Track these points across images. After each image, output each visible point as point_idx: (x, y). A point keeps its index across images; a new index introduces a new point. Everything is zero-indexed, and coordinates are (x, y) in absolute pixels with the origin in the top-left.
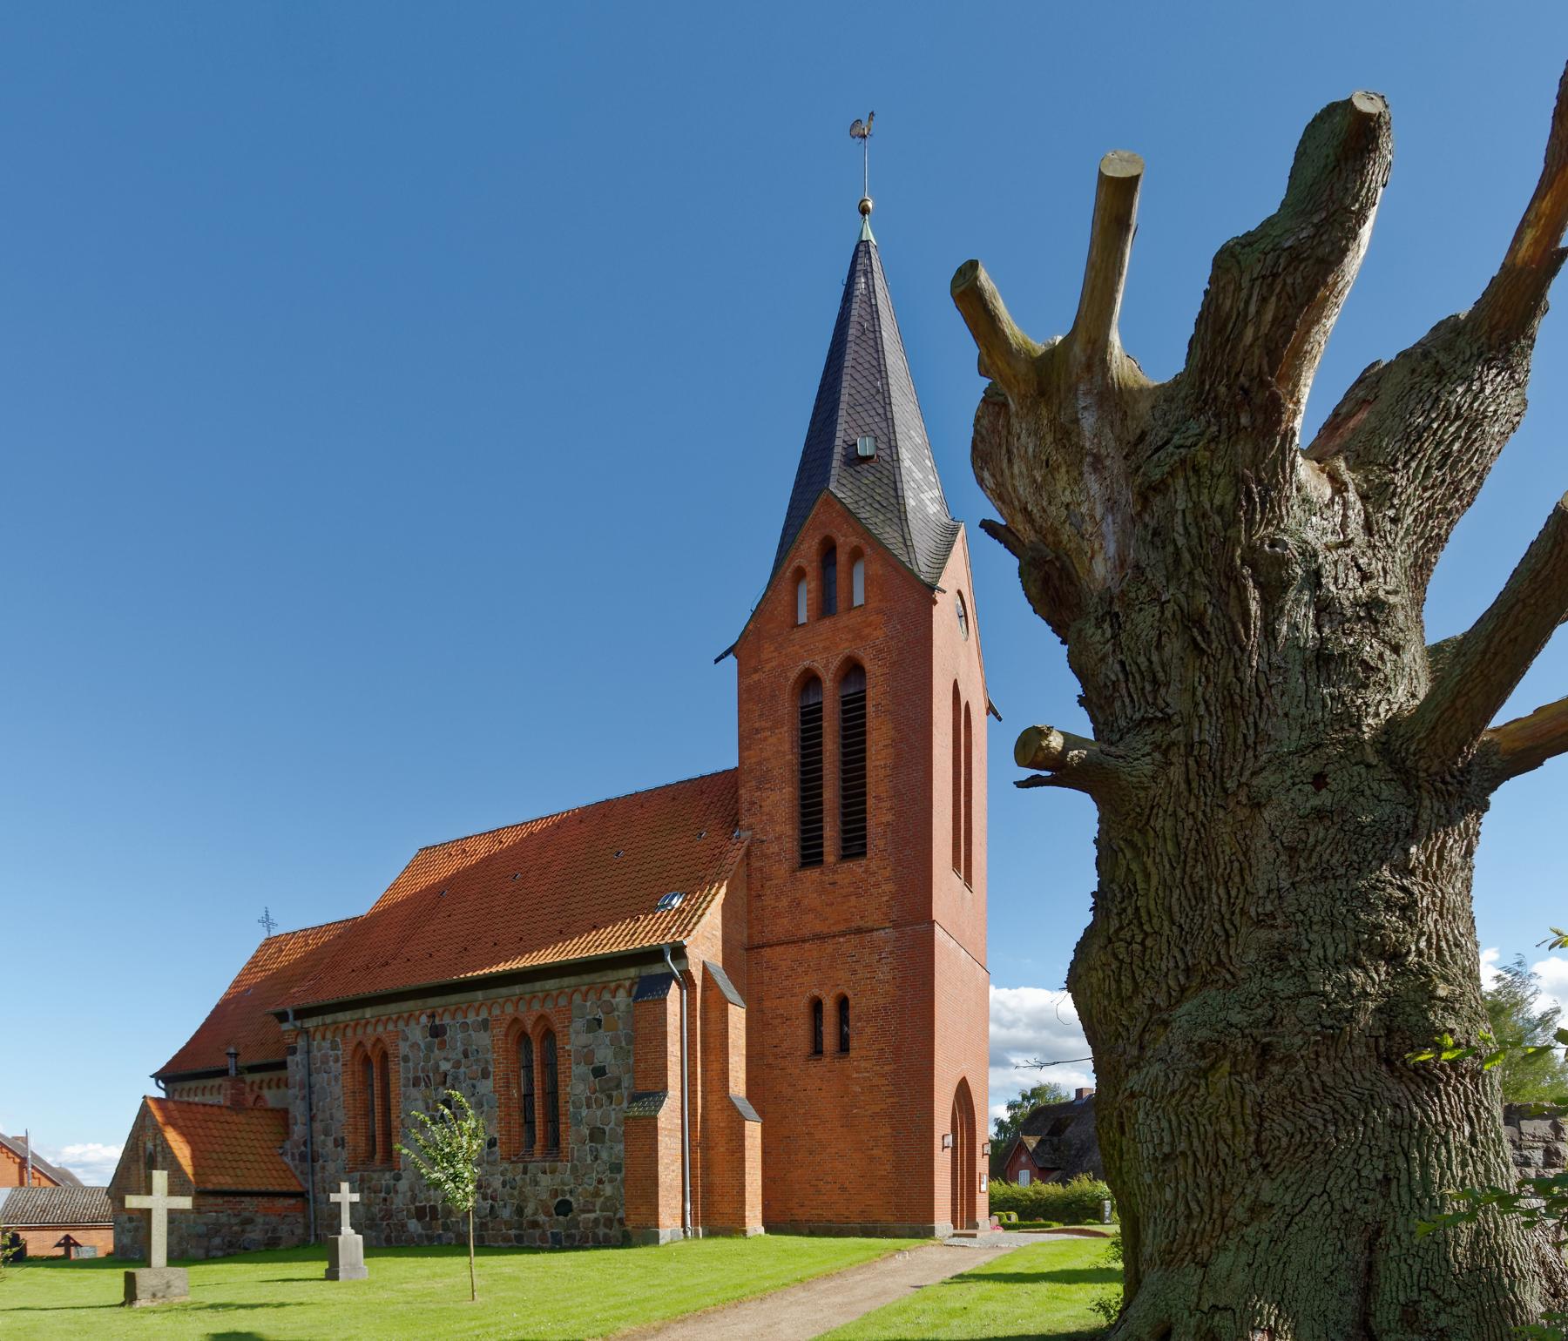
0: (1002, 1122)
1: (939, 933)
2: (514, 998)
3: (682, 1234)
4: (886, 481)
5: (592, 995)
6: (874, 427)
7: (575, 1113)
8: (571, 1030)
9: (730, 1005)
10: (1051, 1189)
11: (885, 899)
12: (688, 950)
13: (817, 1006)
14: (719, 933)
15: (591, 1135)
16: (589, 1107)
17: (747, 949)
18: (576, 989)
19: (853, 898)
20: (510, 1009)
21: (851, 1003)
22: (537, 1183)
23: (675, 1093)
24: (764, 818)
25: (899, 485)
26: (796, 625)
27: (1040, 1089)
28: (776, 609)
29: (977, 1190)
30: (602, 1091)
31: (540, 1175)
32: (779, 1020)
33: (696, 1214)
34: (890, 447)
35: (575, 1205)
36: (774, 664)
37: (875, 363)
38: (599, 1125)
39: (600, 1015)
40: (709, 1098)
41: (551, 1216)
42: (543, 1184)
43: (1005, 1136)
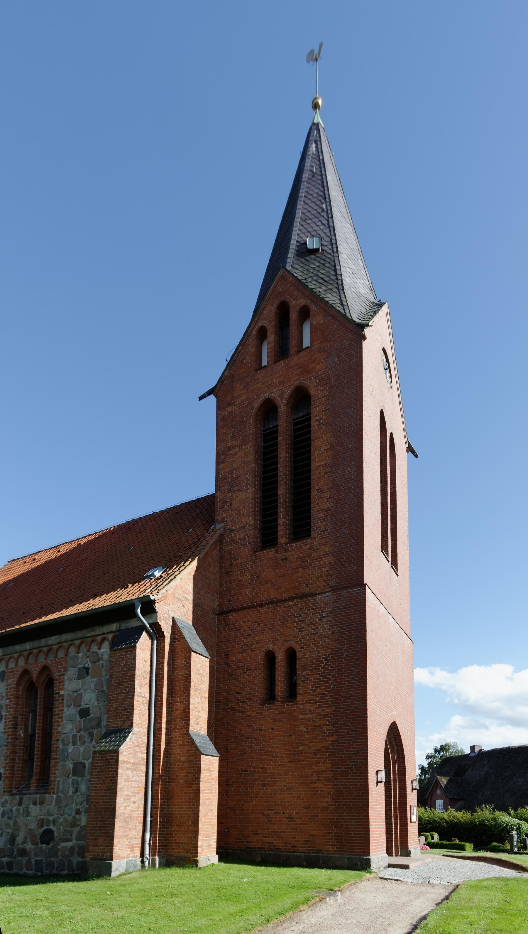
0: (423, 767)
1: (370, 597)
2: (26, 653)
3: (139, 864)
4: (328, 265)
5: (84, 648)
6: (320, 232)
7: (63, 750)
8: (66, 678)
9: (193, 653)
10: (463, 816)
11: (325, 569)
12: (157, 606)
13: (270, 657)
14: (190, 597)
15: (74, 769)
16: (74, 744)
17: (217, 615)
18: (71, 643)
19: (300, 570)
20: (22, 662)
21: (299, 655)
22: (27, 813)
23: (141, 730)
24: (234, 512)
25: (338, 267)
26: (261, 368)
27: (446, 745)
28: (245, 359)
29: (409, 820)
30: (86, 730)
31: (32, 806)
32: (241, 671)
33: (154, 843)
34: (332, 244)
35: (56, 834)
36: (243, 398)
37: (322, 194)
38: (81, 760)
39: (89, 664)
40: (173, 735)
41: (37, 844)
42: (33, 814)
43: (425, 776)
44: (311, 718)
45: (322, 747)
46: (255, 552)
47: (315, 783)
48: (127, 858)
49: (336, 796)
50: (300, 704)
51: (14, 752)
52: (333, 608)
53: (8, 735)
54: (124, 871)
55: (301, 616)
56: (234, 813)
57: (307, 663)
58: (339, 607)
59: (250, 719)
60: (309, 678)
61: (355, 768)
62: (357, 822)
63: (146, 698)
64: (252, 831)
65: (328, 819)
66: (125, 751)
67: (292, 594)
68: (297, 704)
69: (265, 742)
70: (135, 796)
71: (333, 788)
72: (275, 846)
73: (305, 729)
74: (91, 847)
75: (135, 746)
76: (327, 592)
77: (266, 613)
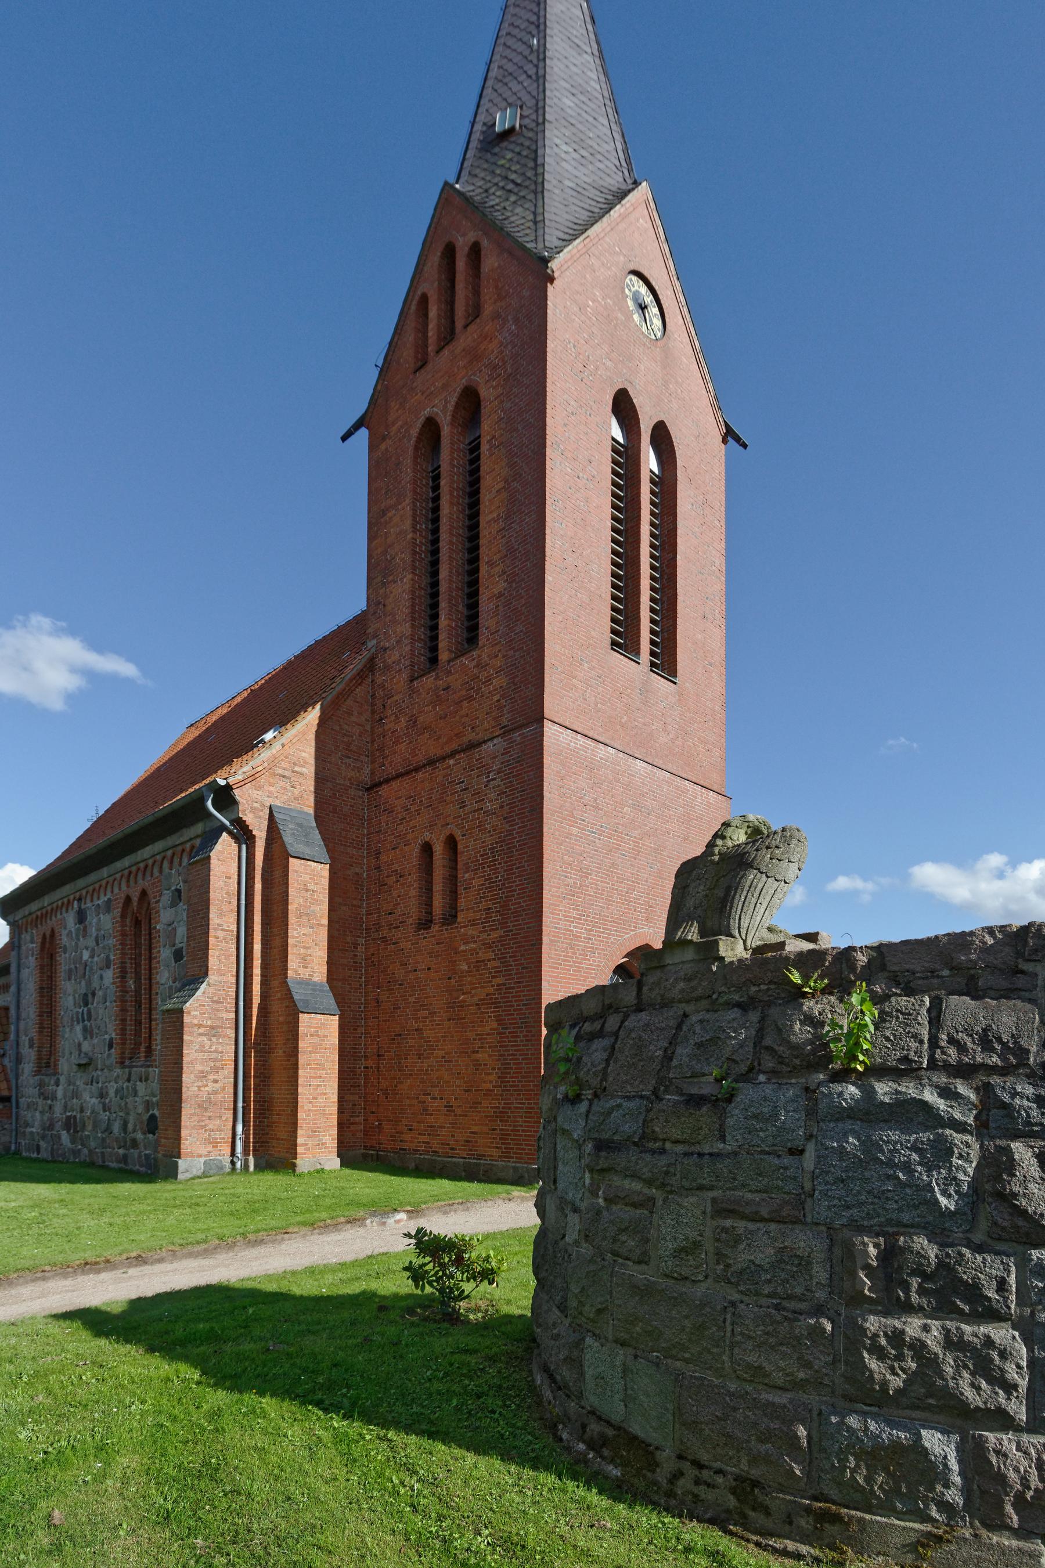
3: (228, 1165)
11: (496, 698)
12: (237, 793)
13: (427, 849)
17: (368, 790)
19: (465, 704)
31: (138, 1083)
44: (475, 949)
45: (487, 995)
46: (412, 681)
47: (478, 1052)
48: (205, 1156)
49: (502, 1073)
50: (461, 927)
51: (124, 1010)
52: (502, 763)
53: (117, 987)
54: (199, 1173)
55: (463, 782)
56: (387, 1098)
57: (470, 859)
58: (509, 761)
59: (404, 954)
60: (472, 883)
61: (526, 1027)
62: (526, 1113)
63: (232, 931)
64: (406, 1125)
65: (492, 1108)
66: (195, 1010)
67: (454, 746)
68: (457, 928)
69: (421, 990)
70: (218, 1072)
71: (499, 1060)
72: (431, 1147)
73: (466, 967)
74: (163, 1140)
75: (213, 1002)
76: (494, 737)
77: (422, 782)
